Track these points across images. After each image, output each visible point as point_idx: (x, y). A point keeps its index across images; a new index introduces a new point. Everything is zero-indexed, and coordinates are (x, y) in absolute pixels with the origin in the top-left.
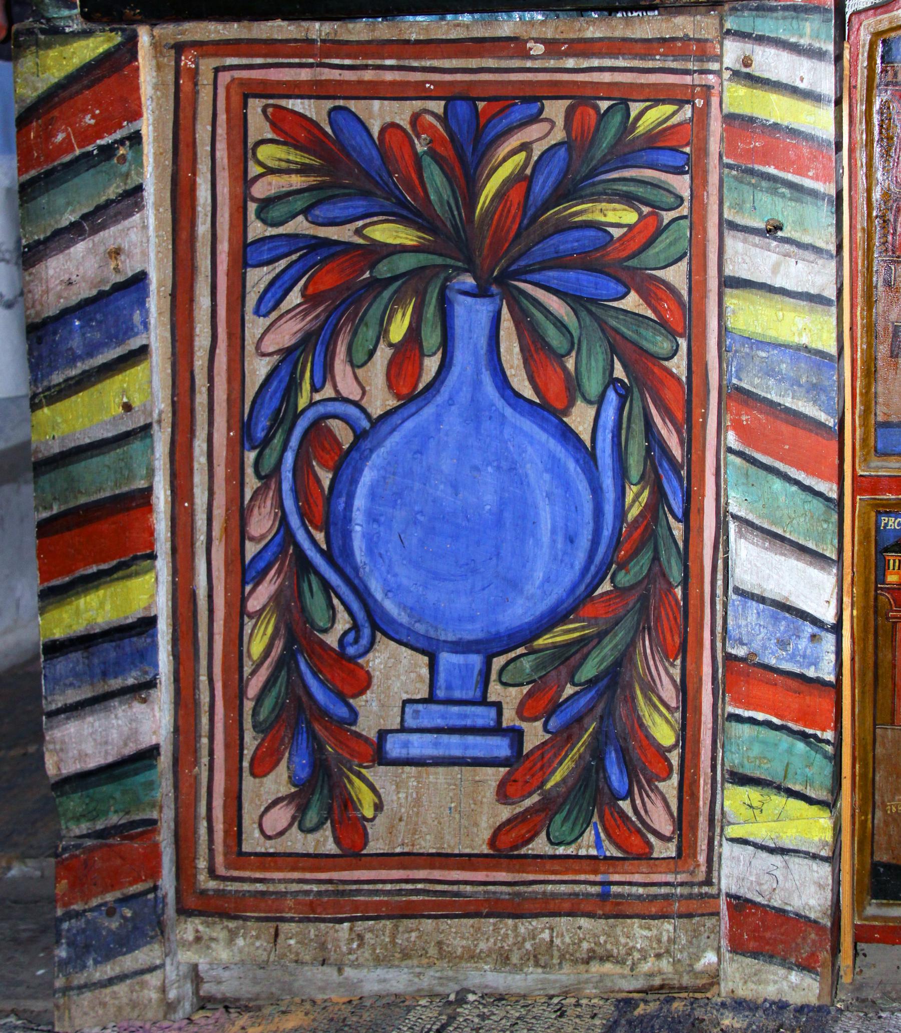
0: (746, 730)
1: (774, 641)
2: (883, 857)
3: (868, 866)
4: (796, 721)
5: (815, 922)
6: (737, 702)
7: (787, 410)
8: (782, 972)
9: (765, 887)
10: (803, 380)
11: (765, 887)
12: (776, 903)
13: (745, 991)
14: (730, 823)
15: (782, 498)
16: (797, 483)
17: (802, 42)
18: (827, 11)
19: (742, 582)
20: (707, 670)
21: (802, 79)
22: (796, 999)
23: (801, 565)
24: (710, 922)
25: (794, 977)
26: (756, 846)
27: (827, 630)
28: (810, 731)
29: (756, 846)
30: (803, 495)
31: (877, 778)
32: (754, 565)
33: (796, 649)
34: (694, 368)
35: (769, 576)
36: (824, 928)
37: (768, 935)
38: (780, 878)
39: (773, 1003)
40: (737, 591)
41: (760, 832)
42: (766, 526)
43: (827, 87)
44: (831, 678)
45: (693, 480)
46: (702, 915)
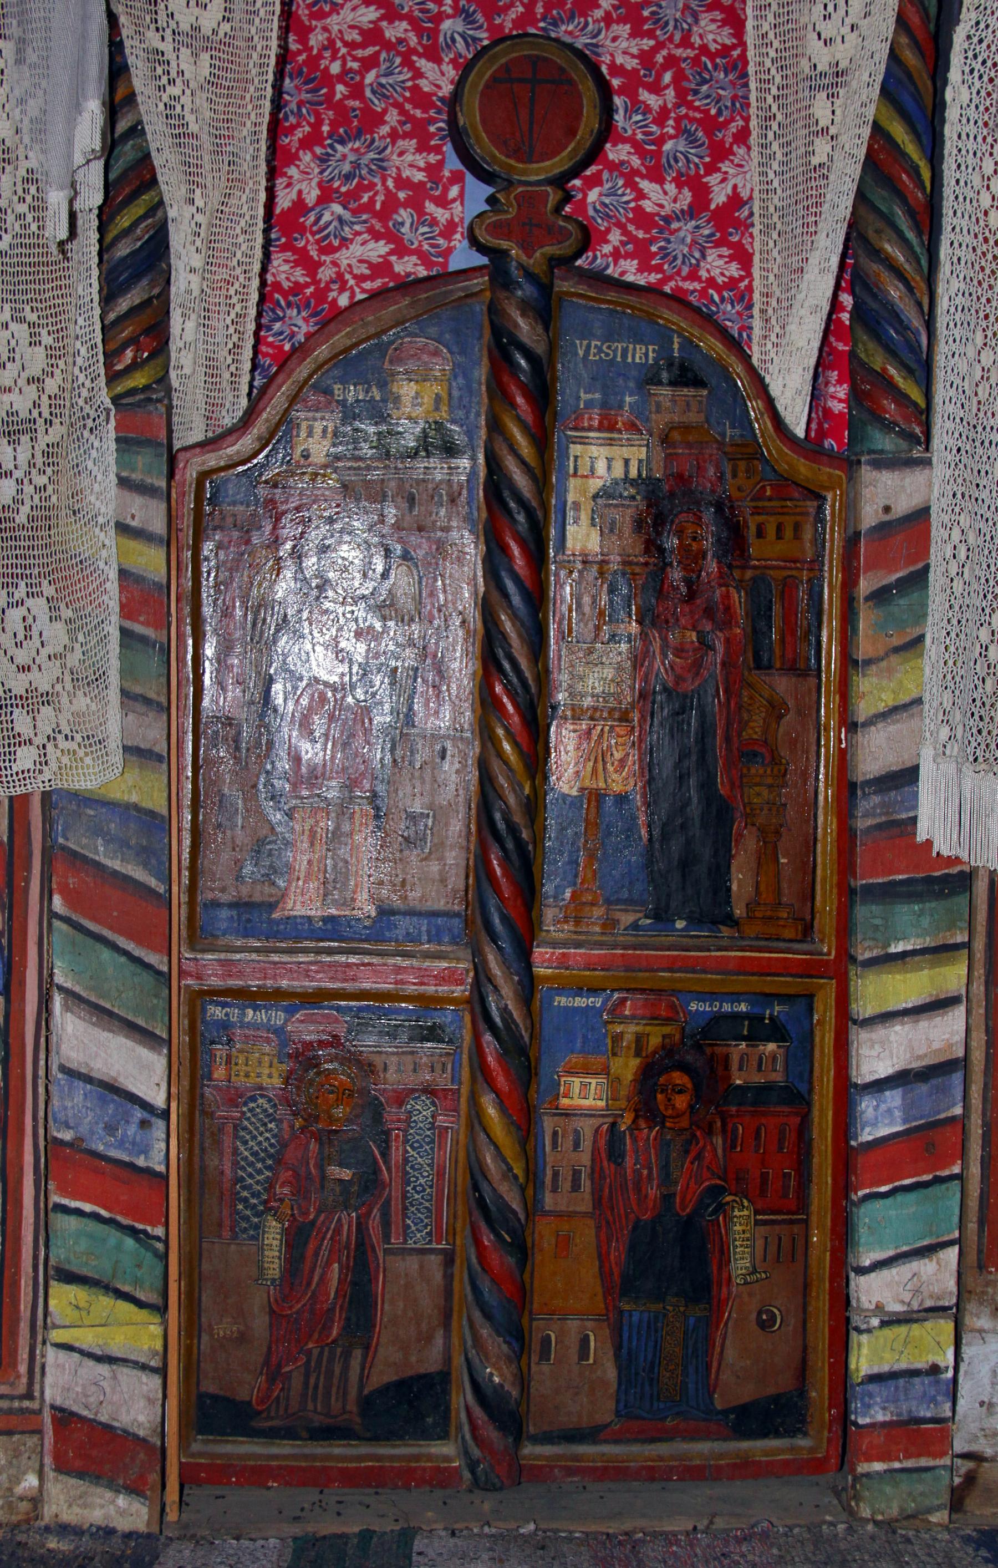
0: (72, 1223)
1: (101, 1125)
2: (210, 1387)
3: (194, 1398)
4: (126, 1215)
5: (144, 1440)
6: (63, 1191)
7: (115, 873)
8: (109, 1495)
9: (92, 1399)
10: (133, 842)
11: (92, 1399)
12: (103, 1418)
13: (70, 1516)
14: (55, 1327)
15: (110, 971)
16: (126, 953)
17: (134, 476)
18: (160, 445)
19: (68, 1058)
20: (28, 1158)
21: (133, 517)
22: (123, 1525)
23: (129, 1043)
24: (32, 1441)
25: (122, 1501)
26: (82, 1352)
27: (158, 1116)
28: (140, 1226)
29: (82, 1352)
30: (132, 967)
31: (204, 1298)
32: (80, 1041)
33: (125, 1135)
34: (16, 826)
35: (97, 1055)
36: (153, 1447)
37: (94, 1453)
38: (108, 1390)
39: (99, 1528)
40: (63, 1069)
41: (86, 1338)
42: (93, 999)
43: (158, 526)
44: (161, 1168)
45: (15, 950)
46: (23, 1432)
